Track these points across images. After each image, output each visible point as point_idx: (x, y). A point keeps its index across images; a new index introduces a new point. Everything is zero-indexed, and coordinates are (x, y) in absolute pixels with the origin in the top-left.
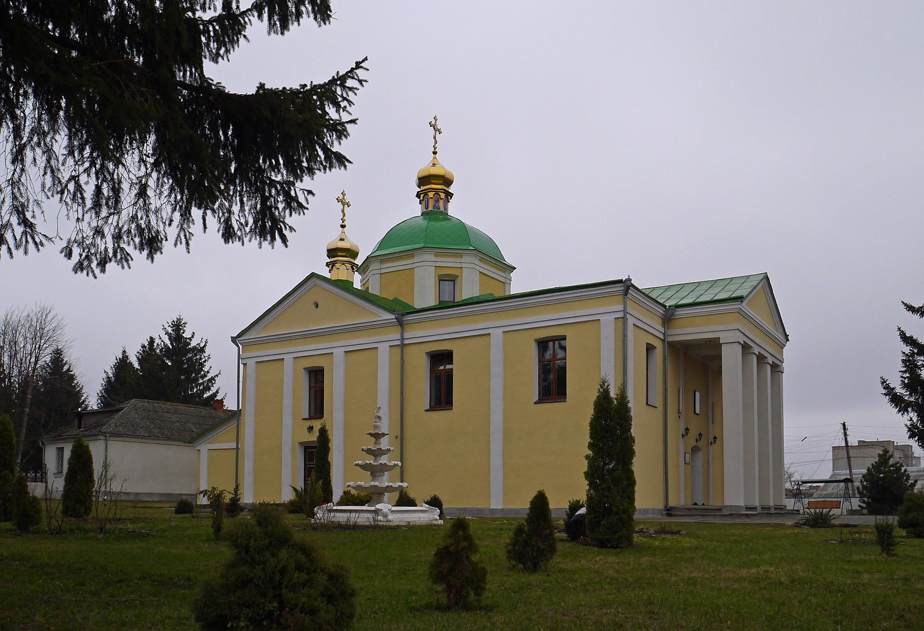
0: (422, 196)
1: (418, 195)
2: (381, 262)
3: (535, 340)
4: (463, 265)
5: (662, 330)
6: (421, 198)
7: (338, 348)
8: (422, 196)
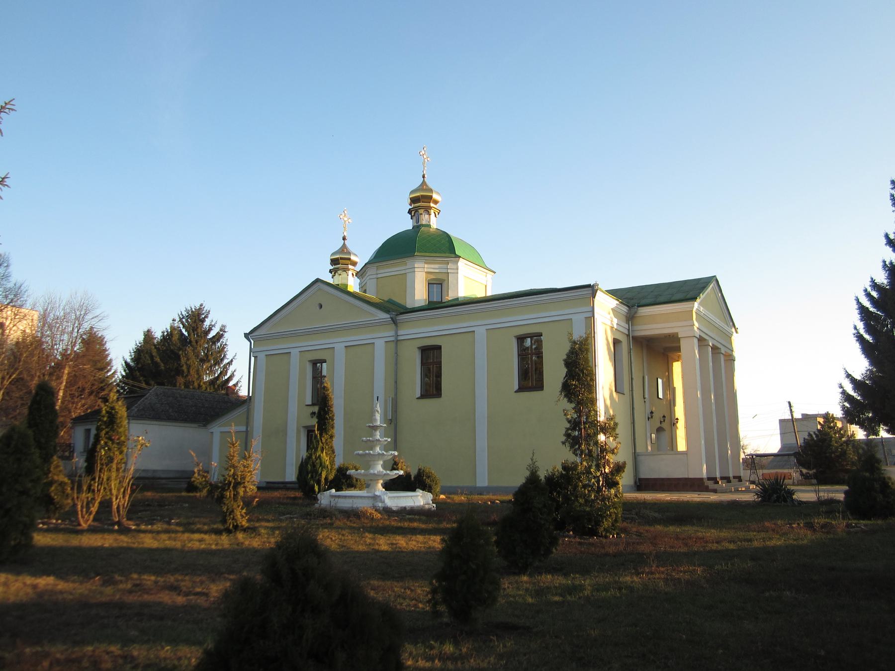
0: (413, 213)
1: (410, 212)
4: (407, 271)
5: (627, 326)
6: (413, 214)
7: (339, 344)
8: (413, 213)
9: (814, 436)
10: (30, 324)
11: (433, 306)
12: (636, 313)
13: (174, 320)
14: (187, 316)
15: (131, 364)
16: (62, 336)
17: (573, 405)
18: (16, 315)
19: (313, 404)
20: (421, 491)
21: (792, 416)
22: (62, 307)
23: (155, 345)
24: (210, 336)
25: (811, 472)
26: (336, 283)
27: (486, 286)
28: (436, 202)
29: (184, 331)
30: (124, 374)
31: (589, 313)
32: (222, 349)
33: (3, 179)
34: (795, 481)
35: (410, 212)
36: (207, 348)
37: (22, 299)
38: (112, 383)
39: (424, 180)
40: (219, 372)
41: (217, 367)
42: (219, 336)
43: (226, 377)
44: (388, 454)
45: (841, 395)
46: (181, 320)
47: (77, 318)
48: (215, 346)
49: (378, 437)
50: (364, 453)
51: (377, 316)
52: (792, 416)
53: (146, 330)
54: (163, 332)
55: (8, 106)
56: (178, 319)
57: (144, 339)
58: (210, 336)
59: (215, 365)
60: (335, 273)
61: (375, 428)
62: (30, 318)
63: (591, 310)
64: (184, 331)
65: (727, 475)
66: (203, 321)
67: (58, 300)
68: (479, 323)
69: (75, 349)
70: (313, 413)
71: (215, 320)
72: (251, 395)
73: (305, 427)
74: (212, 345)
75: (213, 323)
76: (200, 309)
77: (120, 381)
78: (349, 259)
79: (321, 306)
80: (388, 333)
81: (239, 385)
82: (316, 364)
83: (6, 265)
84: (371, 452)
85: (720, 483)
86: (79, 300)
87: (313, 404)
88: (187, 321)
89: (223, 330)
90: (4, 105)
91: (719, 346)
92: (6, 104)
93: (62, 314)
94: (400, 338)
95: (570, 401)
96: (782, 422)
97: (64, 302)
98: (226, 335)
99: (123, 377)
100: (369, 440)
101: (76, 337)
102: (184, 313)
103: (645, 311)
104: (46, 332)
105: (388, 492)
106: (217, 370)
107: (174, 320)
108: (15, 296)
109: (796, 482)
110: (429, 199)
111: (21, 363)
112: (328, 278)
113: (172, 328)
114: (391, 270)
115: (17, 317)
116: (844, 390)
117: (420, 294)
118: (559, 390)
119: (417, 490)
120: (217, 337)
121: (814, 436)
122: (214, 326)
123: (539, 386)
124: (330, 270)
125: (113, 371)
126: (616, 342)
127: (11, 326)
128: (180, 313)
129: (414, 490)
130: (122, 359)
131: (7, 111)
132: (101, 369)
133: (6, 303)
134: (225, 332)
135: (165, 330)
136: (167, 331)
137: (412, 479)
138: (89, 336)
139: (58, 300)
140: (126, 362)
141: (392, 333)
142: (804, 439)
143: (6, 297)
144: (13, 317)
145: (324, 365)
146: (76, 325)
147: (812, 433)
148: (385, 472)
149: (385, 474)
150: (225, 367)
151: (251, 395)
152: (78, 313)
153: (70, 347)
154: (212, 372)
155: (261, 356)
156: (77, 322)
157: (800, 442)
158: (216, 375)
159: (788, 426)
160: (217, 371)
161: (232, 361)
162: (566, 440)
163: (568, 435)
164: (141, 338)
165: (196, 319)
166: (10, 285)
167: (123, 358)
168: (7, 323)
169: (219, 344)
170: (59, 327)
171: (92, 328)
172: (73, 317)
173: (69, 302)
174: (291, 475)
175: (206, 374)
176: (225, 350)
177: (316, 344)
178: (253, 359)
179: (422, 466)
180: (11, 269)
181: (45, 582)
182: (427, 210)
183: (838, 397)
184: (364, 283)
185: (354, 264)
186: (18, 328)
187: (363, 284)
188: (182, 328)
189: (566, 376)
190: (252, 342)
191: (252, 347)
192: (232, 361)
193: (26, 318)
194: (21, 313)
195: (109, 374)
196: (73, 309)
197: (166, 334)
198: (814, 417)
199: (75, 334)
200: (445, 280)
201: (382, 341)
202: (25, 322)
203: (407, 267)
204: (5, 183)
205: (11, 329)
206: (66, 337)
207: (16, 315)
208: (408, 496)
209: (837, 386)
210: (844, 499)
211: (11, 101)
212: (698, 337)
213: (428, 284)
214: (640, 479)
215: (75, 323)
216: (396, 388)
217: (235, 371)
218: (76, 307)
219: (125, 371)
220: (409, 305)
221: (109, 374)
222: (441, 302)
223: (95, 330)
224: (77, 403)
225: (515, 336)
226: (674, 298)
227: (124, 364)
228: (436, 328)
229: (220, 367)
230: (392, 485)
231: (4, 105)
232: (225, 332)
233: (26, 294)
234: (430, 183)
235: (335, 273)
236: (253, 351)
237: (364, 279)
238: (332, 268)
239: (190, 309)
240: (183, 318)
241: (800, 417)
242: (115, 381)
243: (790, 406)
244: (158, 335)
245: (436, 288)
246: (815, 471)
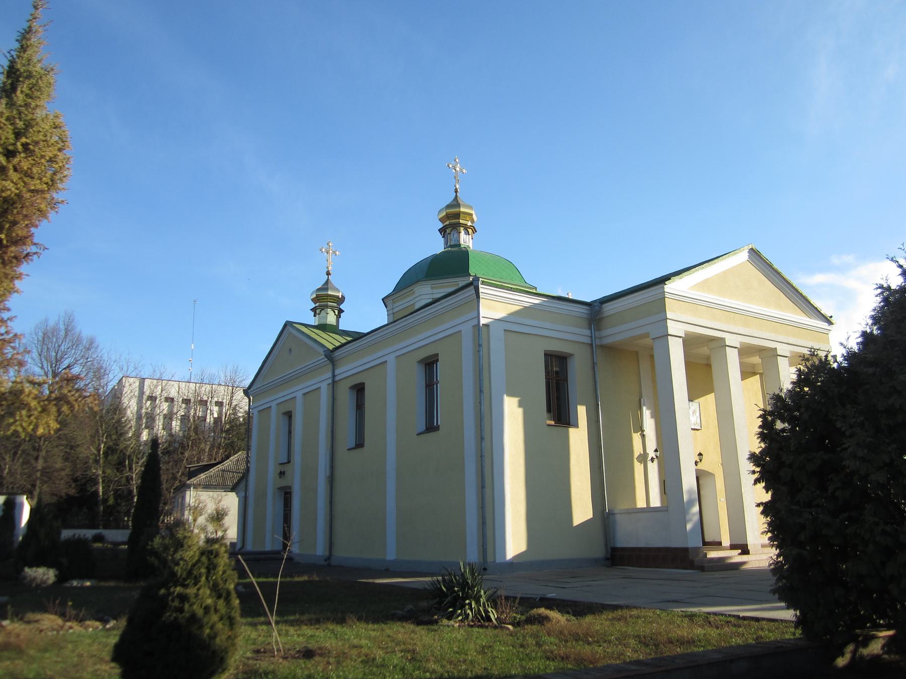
2: (393, 302)
3: (420, 362)
5: (587, 332)
39: (456, 196)
63: (477, 316)
85: (899, 529)
91: (772, 345)
181: (442, 586)
190: (252, 398)
214: (614, 550)
236: (251, 407)
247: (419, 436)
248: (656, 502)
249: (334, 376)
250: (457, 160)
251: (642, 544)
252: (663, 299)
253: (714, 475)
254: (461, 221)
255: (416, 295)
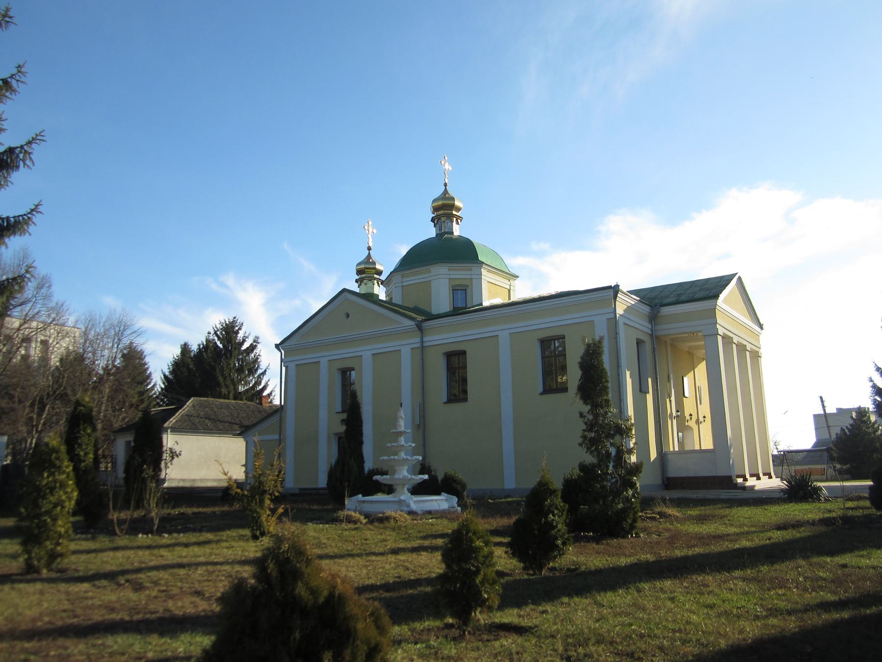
1: (433, 220)
5: (650, 326)
6: (436, 223)
7: (366, 352)
9: (846, 431)
10: (73, 341)
11: (456, 312)
12: (658, 312)
13: (209, 333)
14: (221, 329)
15: (169, 376)
16: (103, 352)
17: (589, 407)
18: (59, 333)
19: (343, 411)
20: (446, 495)
21: (824, 410)
22: (102, 324)
23: (191, 358)
24: (244, 347)
25: (845, 467)
26: (363, 292)
27: (509, 291)
28: (458, 209)
29: (218, 343)
30: (163, 386)
31: (611, 314)
32: (256, 360)
33: (37, 206)
34: (828, 477)
35: (433, 220)
36: (242, 359)
37: (64, 318)
38: (152, 395)
39: (446, 189)
40: (253, 382)
41: (251, 378)
42: (252, 348)
43: (261, 387)
44: (412, 459)
45: (871, 389)
46: (215, 333)
47: (116, 334)
48: (249, 357)
49: (403, 443)
50: (389, 458)
51: (402, 324)
52: (824, 410)
53: (183, 343)
54: (199, 345)
55: (39, 138)
56: (213, 332)
57: (181, 352)
58: (244, 347)
59: (249, 375)
60: (361, 283)
61: (401, 434)
62: (73, 335)
64: (218, 343)
65: (767, 471)
66: (237, 333)
67: (98, 317)
68: (406, 342)
69: (116, 364)
70: (343, 421)
71: (247, 333)
72: (283, 404)
73: (336, 434)
74: (246, 356)
75: (246, 335)
76: (233, 321)
77: (160, 394)
78: (375, 268)
79: (348, 316)
80: (415, 341)
81: (273, 394)
82: (345, 373)
83: (47, 285)
84: (396, 457)
86: (118, 317)
87: (343, 411)
88: (221, 333)
89: (256, 340)
90: (35, 136)
91: (745, 343)
92: (37, 135)
93: (102, 330)
94: (425, 344)
95: (586, 403)
96: (816, 417)
97: (104, 320)
98: (259, 346)
99: (162, 389)
100: (394, 446)
101: (116, 353)
102: (219, 326)
103: (666, 311)
104: (88, 348)
105: (413, 496)
106: (252, 380)
107: (209, 333)
108: (57, 314)
109: (829, 477)
110: (452, 207)
111: (65, 379)
112: (355, 287)
113: (208, 341)
114: (414, 278)
115: (60, 335)
116: (874, 384)
117: (442, 302)
118: (575, 392)
119: (443, 493)
120: (251, 348)
121: (846, 431)
122: (247, 337)
123: (563, 389)
124: (356, 280)
125: (152, 384)
126: (639, 343)
127: (55, 343)
128: (214, 326)
129: (439, 494)
130: (161, 372)
131: (38, 141)
132: (142, 383)
133: (49, 322)
134: (258, 343)
135: (201, 343)
136: (203, 344)
137: (440, 483)
138: (129, 351)
139: (98, 317)
140: (165, 375)
141: (418, 340)
142: (837, 434)
143: (49, 315)
144: (56, 335)
145: (353, 373)
146: (116, 341)
147: (844, 428)
148: (409, 476)
149: (410, 479)
150: (259, 376)
151: (283, 404)
152: (117, 329)
153: (110, 362)
154: (247, 383)
155: (292, 366)
156: (116, 338)
157: (834, 436)
158: (251, 385)
159: (823, 421)
160: (252, 381)
161: (265, 371)
162: (583, 442)
163: (584, 437)
164: (177, 351)
165: (230, 331)
166: (53, 304)
167: (162, 370)
168: (51, 341)
169: (253, 355)
170: (99, 343)
171: (131, 343)
172: (113, 333)
173: (108, 319)
174: (322, 481)
175: (242, 384)
176: (259, 360)
177: (345, 353)
178: (284, 369)
179: (451, 472)
180: (53, 289)
182: (450, 217)
183: (868, 390)
184: (390, 291)
185: (380, 273)
186: (61, 346)
187: (390, 292)
188: (216, 341)
189: (581, 378)
190: (283, 352)
191: (283, 357)
192: (265, 371)
193: (68, 336)
194: (63, 330)
195: (149, 387)
196: (112, 326)
197: (201, 346)
198: (849, 411)
199: (115, 350)
200: (468, 286)
201: (408, 348)
202: (67, 339)
203: (431, 274)
204: (39, 210)
205: (54, 347)
206: (106, 352)
207: (59, 333)
208: (432, 500)
209: (867, 380)
210: (869, 495)
211: (41, 132)
212: (722, 334)
213: (453, 290)
214: (668, 478)
215: (114, 339)
216: (423, 393)
217: (269, 381)
218: (116, 322)
219: (164, 383)
220: (435, 312)
221: (149, 387)
222: (466, 308)
223: (135, 345)
224: (119, 416)
225: (338, 369)
226: (697, 296)
227: (163, 377)
228: (542, 321)
229: (254, 378)
230: (418, 490)
231: (35, 136)
232: (258, 343)
233: (68, 312)
234: (452, 192)
235: (361, 283)
237: (391, 286)
238: (358, 277)
239: (224, 321)
240: (218, 330)
241: (835, 411)
242: (155, 394)
243: (822, 401)
244: (194, 348)
245: (460, 295)
246: (848, 466)
247: (819, 400)
248: (677, 449)
249: (422, 342)
250: (446, 158)
251: (691, 474)
252: (713, 310)
253: (693, 429)
254: (454, 213)
255: (431, 274)
